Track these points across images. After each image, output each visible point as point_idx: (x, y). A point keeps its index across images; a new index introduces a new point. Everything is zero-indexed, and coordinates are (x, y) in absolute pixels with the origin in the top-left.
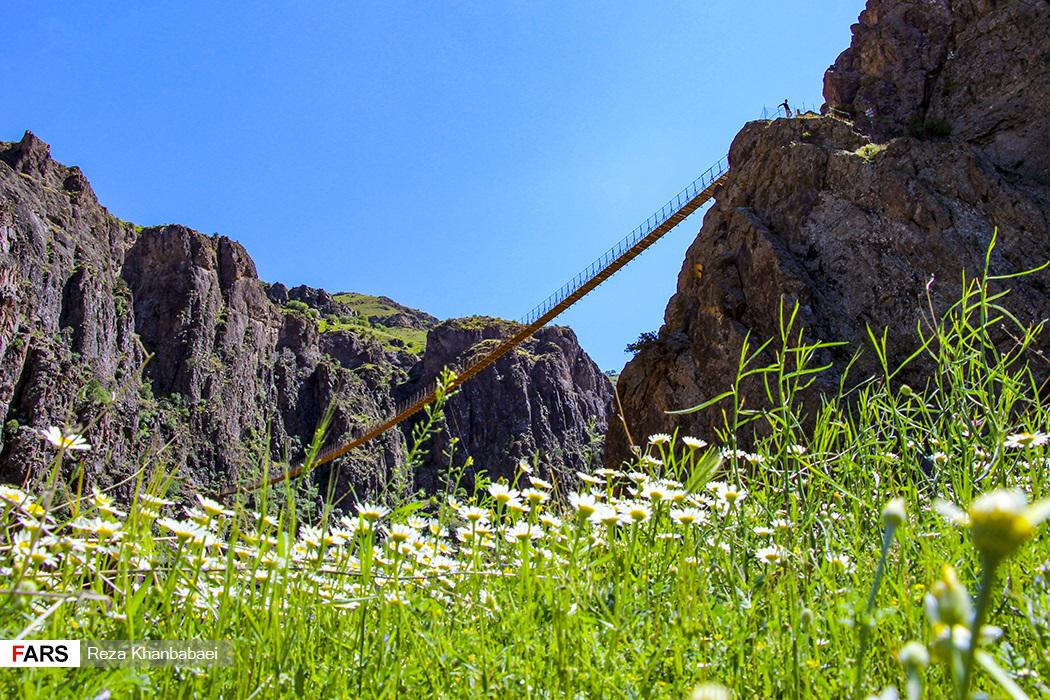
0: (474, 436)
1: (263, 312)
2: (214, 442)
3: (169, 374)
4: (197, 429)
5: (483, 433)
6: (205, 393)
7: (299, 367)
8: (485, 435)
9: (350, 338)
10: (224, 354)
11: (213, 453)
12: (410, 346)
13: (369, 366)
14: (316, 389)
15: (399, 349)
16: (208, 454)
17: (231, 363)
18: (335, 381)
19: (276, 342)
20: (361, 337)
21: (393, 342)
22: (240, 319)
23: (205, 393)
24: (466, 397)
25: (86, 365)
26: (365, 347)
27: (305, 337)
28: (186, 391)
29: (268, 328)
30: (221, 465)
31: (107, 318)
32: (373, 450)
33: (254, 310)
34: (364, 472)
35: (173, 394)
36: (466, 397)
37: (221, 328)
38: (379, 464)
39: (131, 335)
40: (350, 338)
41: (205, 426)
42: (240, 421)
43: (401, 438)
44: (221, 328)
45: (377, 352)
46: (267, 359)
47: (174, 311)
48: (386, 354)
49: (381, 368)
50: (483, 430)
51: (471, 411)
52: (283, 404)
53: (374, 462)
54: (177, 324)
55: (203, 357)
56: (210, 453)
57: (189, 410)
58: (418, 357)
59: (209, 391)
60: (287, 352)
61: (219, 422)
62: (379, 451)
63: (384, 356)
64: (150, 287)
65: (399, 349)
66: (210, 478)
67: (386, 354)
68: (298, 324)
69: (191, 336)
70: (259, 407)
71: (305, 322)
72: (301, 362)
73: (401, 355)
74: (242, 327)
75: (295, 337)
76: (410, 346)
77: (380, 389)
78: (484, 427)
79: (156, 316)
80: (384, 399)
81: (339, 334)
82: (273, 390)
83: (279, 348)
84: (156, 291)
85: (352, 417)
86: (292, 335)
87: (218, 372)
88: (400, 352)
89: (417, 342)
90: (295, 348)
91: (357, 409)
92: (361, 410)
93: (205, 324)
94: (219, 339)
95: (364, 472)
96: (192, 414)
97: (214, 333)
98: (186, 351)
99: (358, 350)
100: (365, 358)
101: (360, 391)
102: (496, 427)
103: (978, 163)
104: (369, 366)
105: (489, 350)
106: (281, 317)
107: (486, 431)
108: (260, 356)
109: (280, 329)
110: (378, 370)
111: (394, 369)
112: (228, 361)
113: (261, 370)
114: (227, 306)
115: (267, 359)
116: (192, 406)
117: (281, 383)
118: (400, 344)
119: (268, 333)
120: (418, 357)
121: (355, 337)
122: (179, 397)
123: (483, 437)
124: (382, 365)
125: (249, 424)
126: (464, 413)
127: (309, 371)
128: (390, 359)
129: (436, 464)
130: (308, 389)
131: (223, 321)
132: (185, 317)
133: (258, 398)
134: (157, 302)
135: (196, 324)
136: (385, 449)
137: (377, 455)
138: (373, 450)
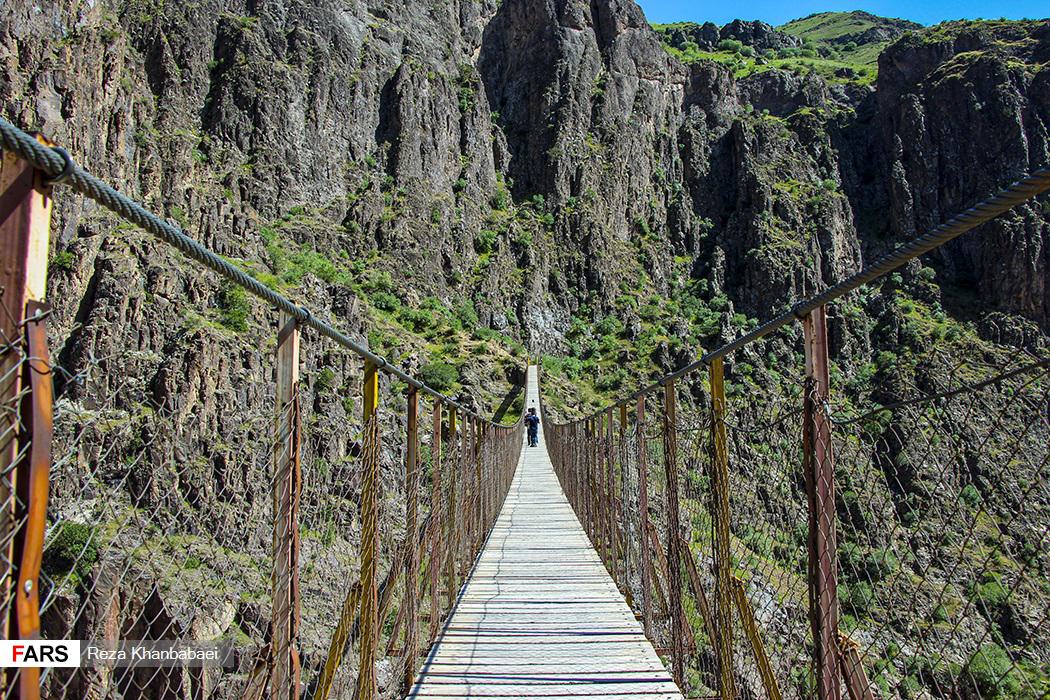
0: (946, 190)
1: (657, 67)
2: (585, 250)
3: (531, 174)
4: (565, 237)
5: (958, 186)
6: (575, 188)
7: (710, 128)
8: (961, 187)
9: (781, 77)
10: (603, 132)
11: (583, 266)
12: (862, 74)
13: (805, 111)
14: (732, 153)
15: (847, 81)
16: (578, 269)
17: (611, 142)
18: (753, 141)
19: (681, 101)
20: (796, 74)
21: (840, 73)
22: (626, 83)
23: (575, 188)
24: (932, 138)
25: (401, 189)
26: (801, 87)
27: (716, 88)
28: (550, 189)
29: (668, 86)
30: (594, 282)
31: (438, 119)
32: (801, 229)
33: (644, 66)
34: (786, 264)
35: (535, 197)
36: (932, 138)
37: (598, 100)
38: (810, 248)
39: (484, 129)
40: (781, 77)
41: (577, 234)
42: (627, 214)
43: (844, 205)
44: (598, 100)
45: (816, 91)
46: (667, 125)
47: (543, 85)
48: (831, 90)
49: (821, 111)
50: (957, 181)
51: (940, 157)
52: (691, 181)
53: (802, 247)
54: (543, 104)
55: (574, 142)
56: (579, 266)
57: (554, 215)
58: (871, 87)
59: (580, 184)
60: (696, 110)
61: (592, 225)
62: (810, 230)
63: (828, 93)
64: (518, 64)
65: (847, 81)
66: (580, 300)
67: (831, 90)
68: (706, 73)
69: (559, 118)
70: (656, 189)
71: (715, 70)
72: (712, 121)
73: (849, 89)
74: (629, 93)
75: (704, 91)
76: (862, 74)
77: (818, 139)
78: (960, 176)
79: (525, 97)
80: (824, 152)
81: (767, 75)
82: (676, 163)
83: (686, 107)
84: (525, 67)
85: (776, 186)
86: (701, 88)
87: (593, 157)
88: (848, 84)
89: (865, 65)
90: (706, 104)
91: (783, 173)
92: (789, 174)
93: (576, 98)
94: (596, 113)
95: (786, 264)
96: (557, 218)
97: (590, 106)
98: (551, 138)
99: (792, 91)
100: (800, 100)
101: (788, 148)
102: (975, 177)
103: (395, 183)
104: (805, 111)
105: (962, 69)
106: (683, 69)
107: (961, 182)
108: (657, 124)
109: (685, 85)
110: (817, 114)
111: (840, 108)
112: (608, 140)
113: (659, 142)
114: (608, 70)
115: (667, 125)
116: (558, 209)
117: (686, 154)
118: (849, 73)
119: (667, 93)
120: (871, 87)
121: (787, 75)
122: (541, 199)
123: (957, 190)
124: (823, 107)
125: (642, 217)
126: (930, 161)
127: (723, 131)
128: (835, 96)
129: (893, 234)
130: (722, 154)
131: (600, 90)
132: (552, 96)
133: (655, 179)
134: (526, 81)
135: (564, 102)
136: (818, 227)
137: (807, 236)
138: (801, 229)
